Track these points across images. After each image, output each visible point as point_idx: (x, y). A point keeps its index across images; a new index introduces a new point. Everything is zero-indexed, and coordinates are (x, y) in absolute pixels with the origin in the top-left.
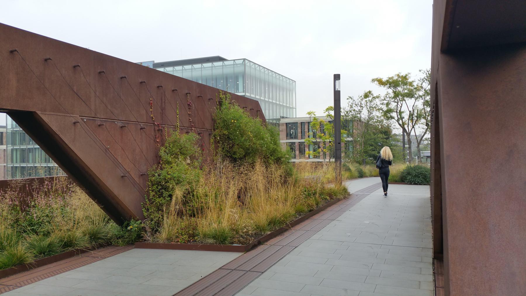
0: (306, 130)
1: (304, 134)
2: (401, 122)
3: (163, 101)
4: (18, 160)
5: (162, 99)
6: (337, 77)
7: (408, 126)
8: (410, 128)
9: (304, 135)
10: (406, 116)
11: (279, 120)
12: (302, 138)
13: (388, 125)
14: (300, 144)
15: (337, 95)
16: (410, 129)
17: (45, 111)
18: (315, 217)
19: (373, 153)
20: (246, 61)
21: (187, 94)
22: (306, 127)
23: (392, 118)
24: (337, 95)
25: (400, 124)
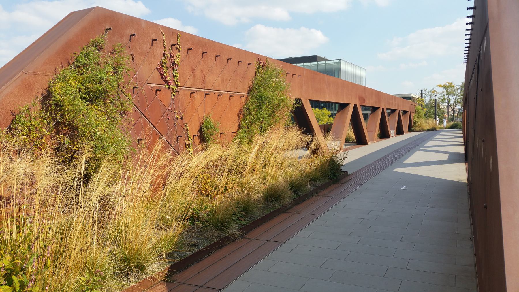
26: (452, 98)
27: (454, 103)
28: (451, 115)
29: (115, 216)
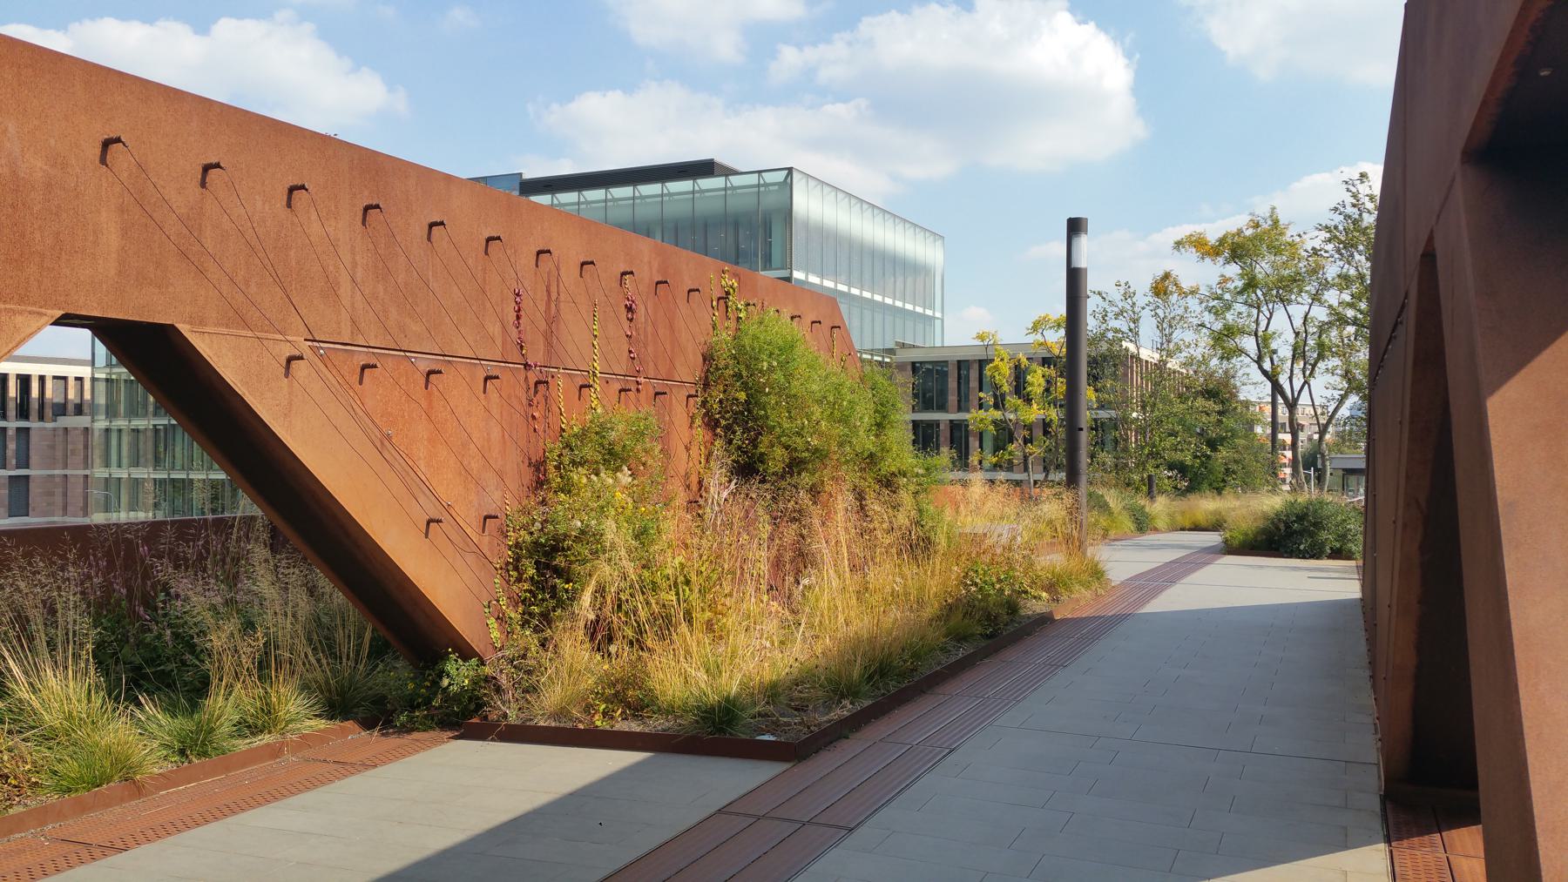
0: (974, 384)
1: (967, 396)
2: (1267, 365)
3: (554, 297)
4: (125, 461)
5: (548, 291)
6: (1075, 227)
7: (1291, 379)
8: (1297, 384)
9: (967, 399)
10: (1283, 347)
11: (890, 351)
12: (960, 409)
13: (1226, 372)
14: (955, 426)
15: (1075, 277)
16: (1297, 387)
17: (202, 323)
18: (1012, 654)
19: (1178, 456)
20: (795, 174)
21: (624, 274)
22: (974, 374)
23: (1241, 351)
24: (1075, 277)
25: (1264, 372)
26: (1283, 324)
27: (1298, 353)
28: (1310, 439)
29: (358, 653)
